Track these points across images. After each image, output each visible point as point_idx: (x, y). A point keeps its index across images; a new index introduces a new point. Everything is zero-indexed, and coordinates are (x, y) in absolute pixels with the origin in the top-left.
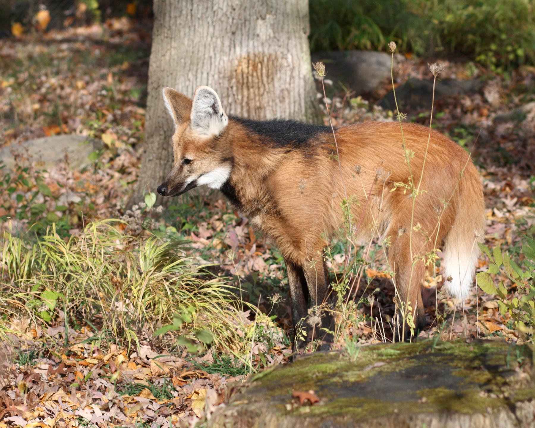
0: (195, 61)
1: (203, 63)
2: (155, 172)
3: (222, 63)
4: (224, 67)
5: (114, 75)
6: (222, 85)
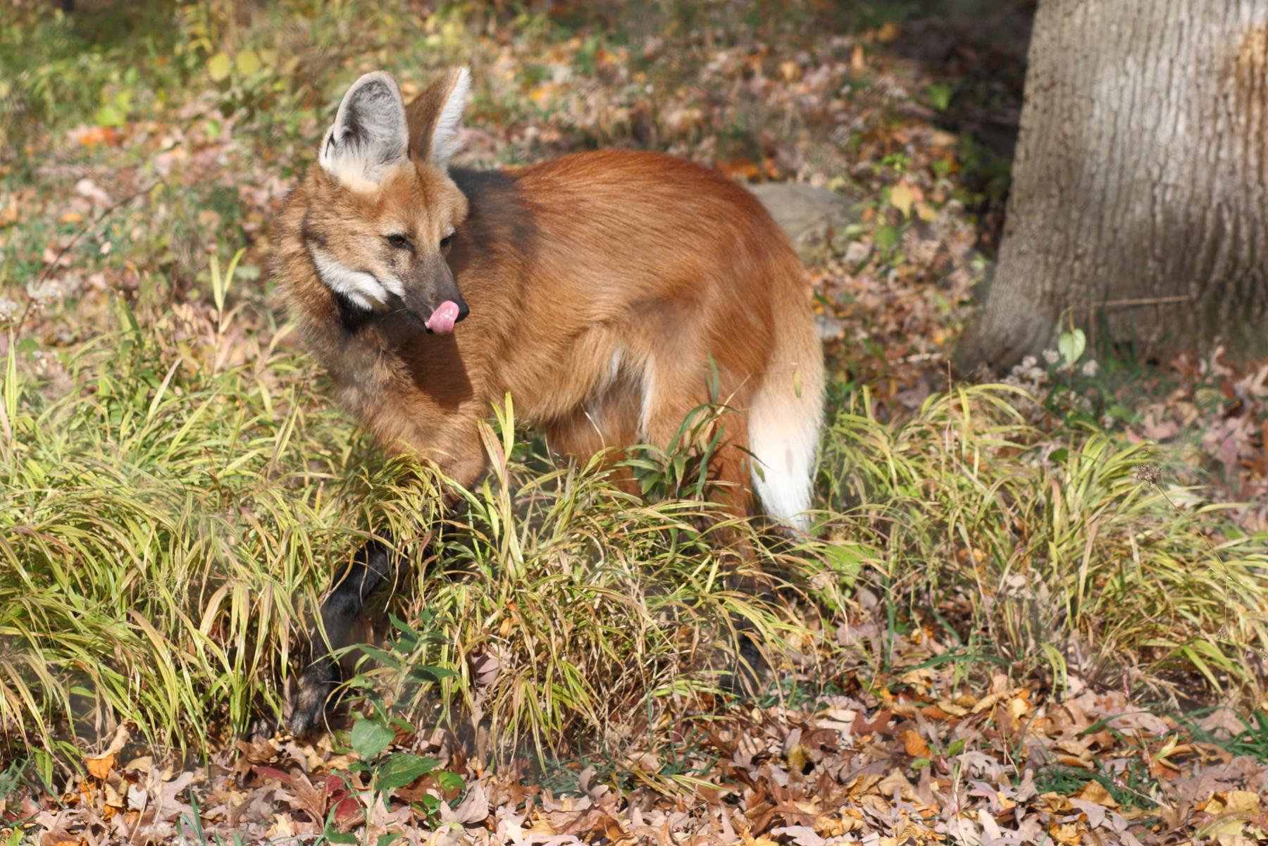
0: (1144, 31)
1: (1162, 37)
2: (1033, 280)
3: (1205, 39)
4: (1210, 48)
5: (867, 51)
6: (1202, 89)
